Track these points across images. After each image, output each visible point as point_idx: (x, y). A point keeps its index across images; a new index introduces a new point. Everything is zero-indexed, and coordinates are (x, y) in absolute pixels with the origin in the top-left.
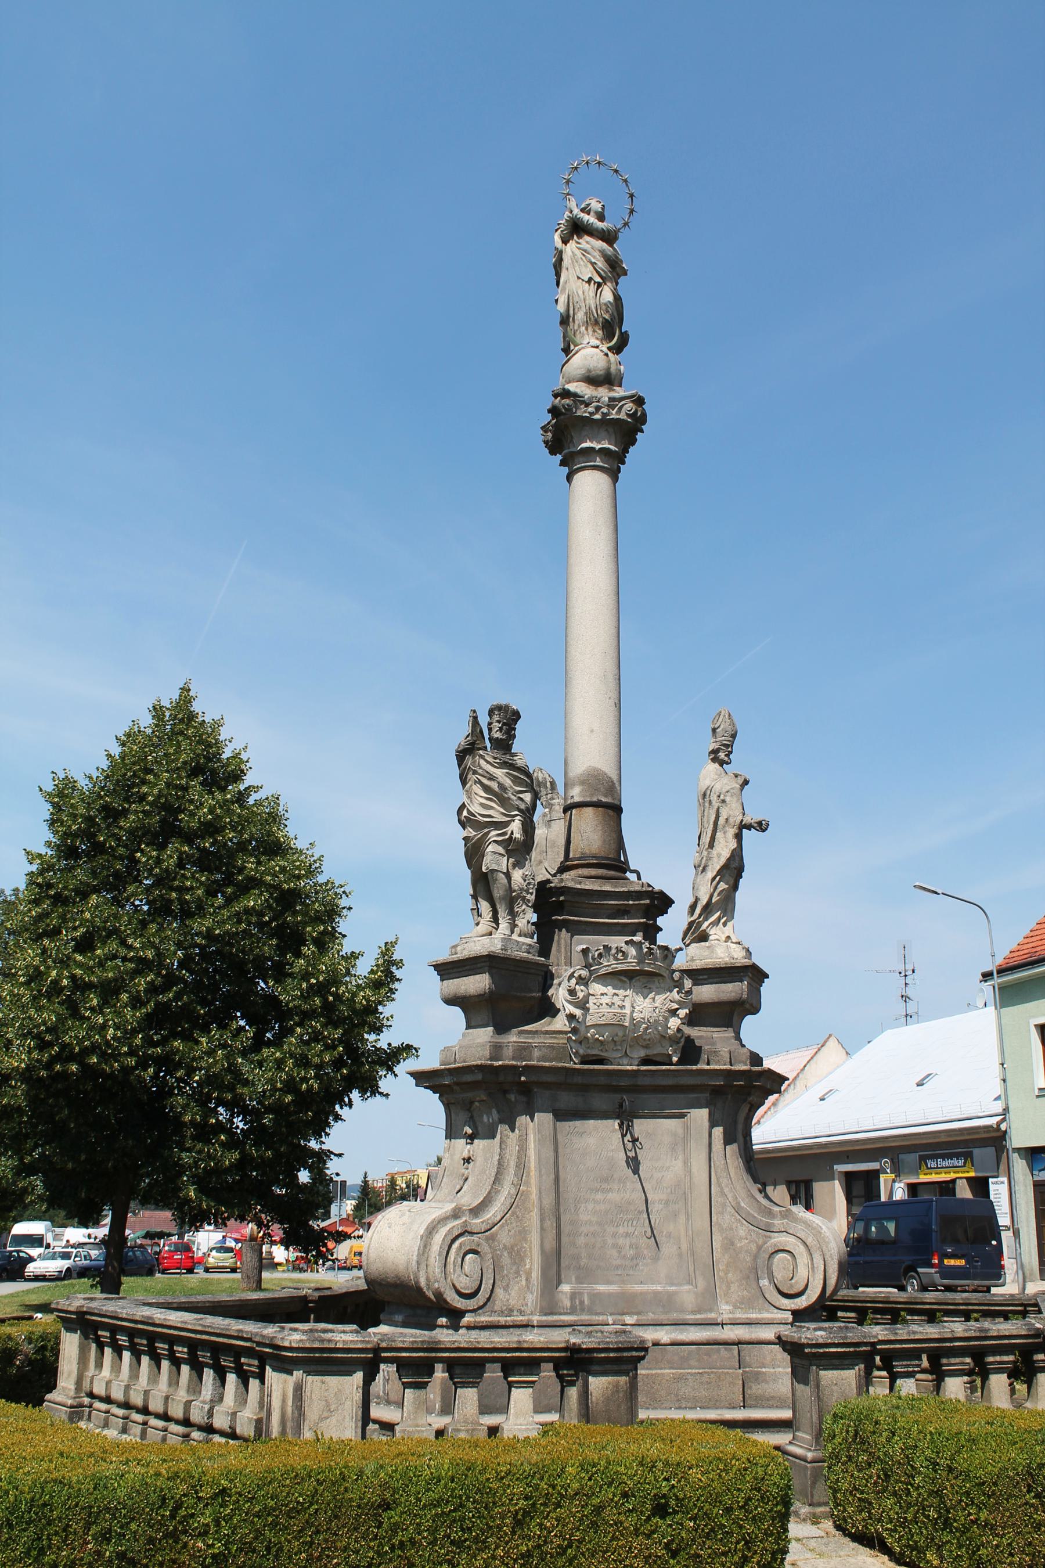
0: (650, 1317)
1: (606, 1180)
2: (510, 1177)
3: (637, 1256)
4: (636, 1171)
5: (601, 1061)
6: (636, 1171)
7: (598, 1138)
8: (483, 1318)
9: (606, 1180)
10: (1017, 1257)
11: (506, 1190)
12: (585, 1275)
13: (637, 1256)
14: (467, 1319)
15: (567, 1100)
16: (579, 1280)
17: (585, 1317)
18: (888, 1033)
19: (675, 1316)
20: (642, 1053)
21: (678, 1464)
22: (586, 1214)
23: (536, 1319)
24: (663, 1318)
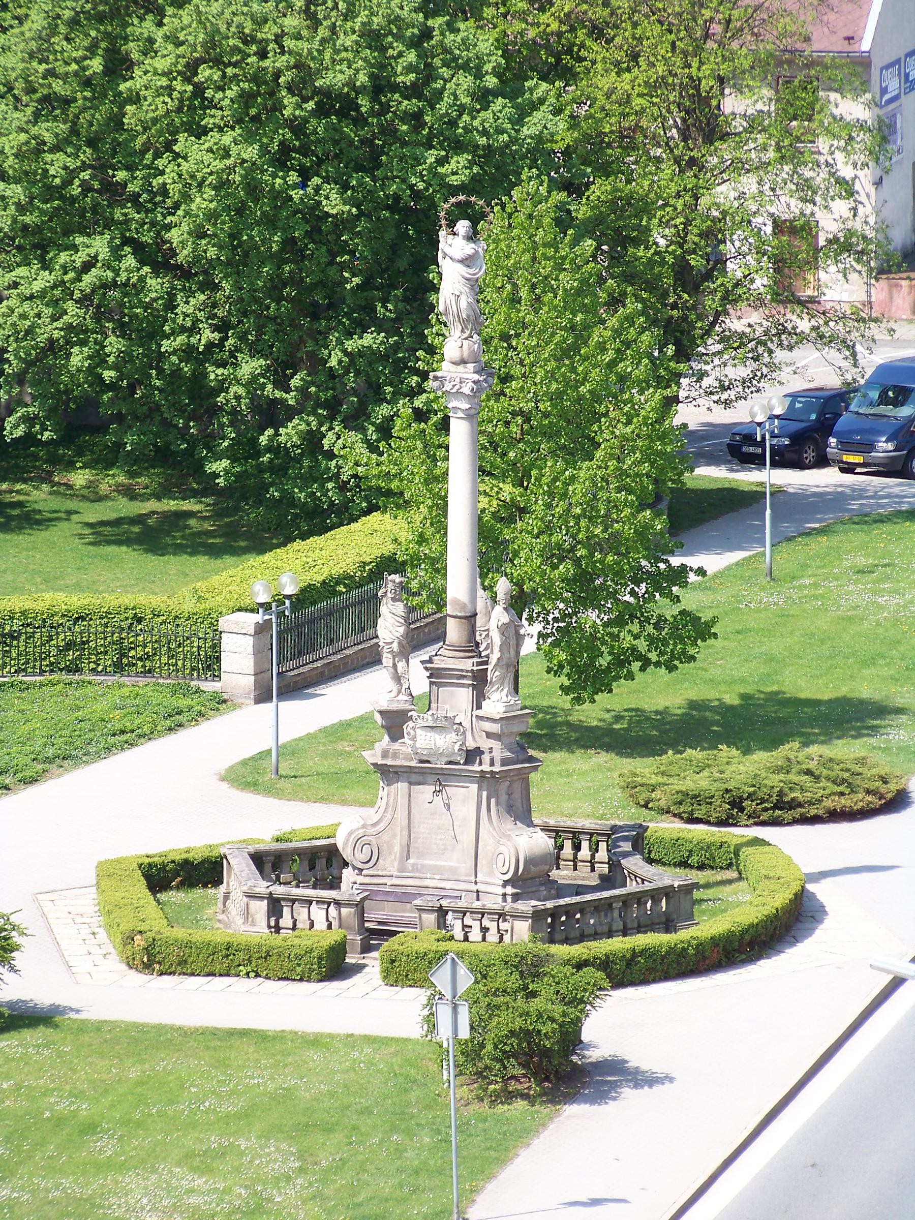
0: (446, 877)
1: (433, 814)
2: (390, 811)
3: (445, 849)
4: (449, 809)
5: (428, 762)
6: (449, 809)
7: (425, 792)
8: (371, 872)
9: (433, 814)
10: (891, 487)
11: (389, 816)
12: (421, 855)
13: (445, 849)
14: (364, 872)
15: (414, 778)
16: (418, 858)
17: (417, 875)
18: (826, 698)
19: (456, 877)
20: (446, 759)
21: (205, 1152)
22: (422, 829)
23: (395, 873)
24: (451, 877)
